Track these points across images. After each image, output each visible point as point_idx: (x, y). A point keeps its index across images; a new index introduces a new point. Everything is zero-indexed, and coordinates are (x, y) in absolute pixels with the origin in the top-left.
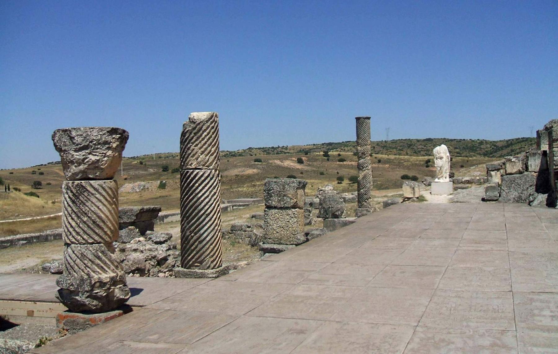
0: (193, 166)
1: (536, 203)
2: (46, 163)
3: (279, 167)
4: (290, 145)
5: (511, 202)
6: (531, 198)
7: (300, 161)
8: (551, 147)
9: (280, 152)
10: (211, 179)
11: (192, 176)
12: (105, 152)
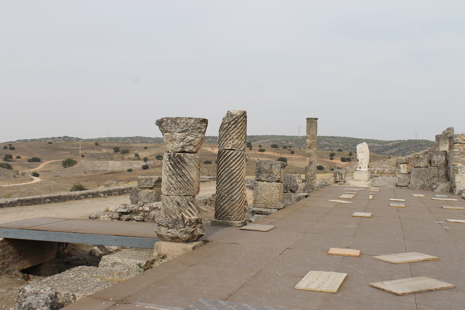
0: (229, 148)
1: (438, 190)
2: (15, 140)
5: (418, 188)
6: (434, 186)
8: (451, 147)
10: (242, 157)
11: (228, 154)
12: (197, 134)
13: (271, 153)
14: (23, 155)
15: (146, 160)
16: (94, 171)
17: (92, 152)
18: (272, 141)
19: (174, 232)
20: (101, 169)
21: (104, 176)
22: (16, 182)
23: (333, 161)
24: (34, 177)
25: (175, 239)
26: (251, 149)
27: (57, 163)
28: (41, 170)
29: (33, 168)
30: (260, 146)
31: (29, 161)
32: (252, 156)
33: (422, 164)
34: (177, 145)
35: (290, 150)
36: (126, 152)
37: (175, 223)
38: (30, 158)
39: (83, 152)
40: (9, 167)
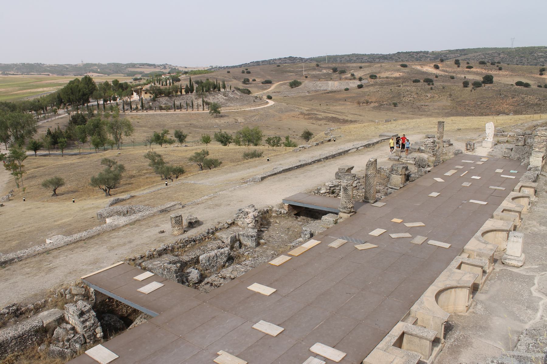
3: (419, 71)
4: (430, 51)
7: (437, 67)
9: (420, 57)
13: (479, 70)
14: (257, 78)
15: (360, 79)
16: (316, 91)
17: (314, 73)
18: (483, 54)
19: (344, 210)
20: (322, 89)
21: (324, 95)
22: (256, 106)
23: (543, 76)
24: (268, 101)
25: (345, 212)
26: (458, 67)
27: (285, 84)
28: (273, 91)
29: (266, 89)
30: (468, 63)
31: (263, 83)
32: (459, 73)
33: (520, 144)
34: (346, 184)
35: (498, 66)
36: (343, 72)
37: (344, 208)
38: (263, 80)
39: (306, 73)
40: (249, 92)
